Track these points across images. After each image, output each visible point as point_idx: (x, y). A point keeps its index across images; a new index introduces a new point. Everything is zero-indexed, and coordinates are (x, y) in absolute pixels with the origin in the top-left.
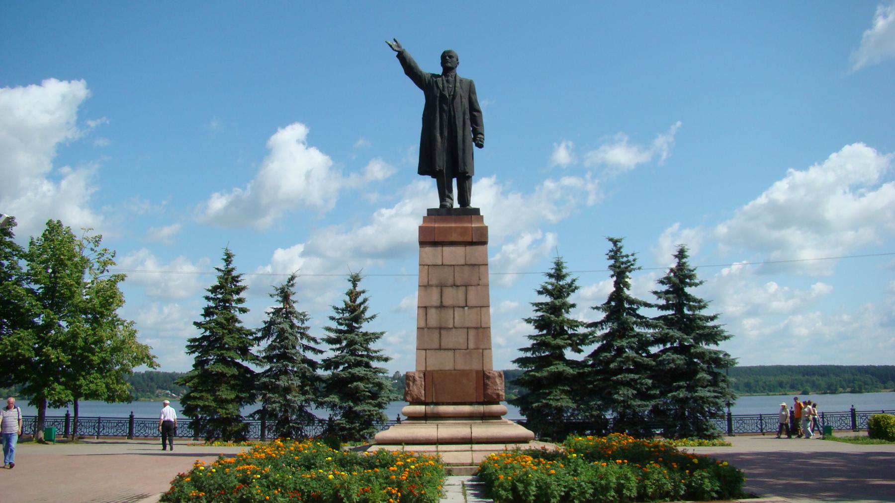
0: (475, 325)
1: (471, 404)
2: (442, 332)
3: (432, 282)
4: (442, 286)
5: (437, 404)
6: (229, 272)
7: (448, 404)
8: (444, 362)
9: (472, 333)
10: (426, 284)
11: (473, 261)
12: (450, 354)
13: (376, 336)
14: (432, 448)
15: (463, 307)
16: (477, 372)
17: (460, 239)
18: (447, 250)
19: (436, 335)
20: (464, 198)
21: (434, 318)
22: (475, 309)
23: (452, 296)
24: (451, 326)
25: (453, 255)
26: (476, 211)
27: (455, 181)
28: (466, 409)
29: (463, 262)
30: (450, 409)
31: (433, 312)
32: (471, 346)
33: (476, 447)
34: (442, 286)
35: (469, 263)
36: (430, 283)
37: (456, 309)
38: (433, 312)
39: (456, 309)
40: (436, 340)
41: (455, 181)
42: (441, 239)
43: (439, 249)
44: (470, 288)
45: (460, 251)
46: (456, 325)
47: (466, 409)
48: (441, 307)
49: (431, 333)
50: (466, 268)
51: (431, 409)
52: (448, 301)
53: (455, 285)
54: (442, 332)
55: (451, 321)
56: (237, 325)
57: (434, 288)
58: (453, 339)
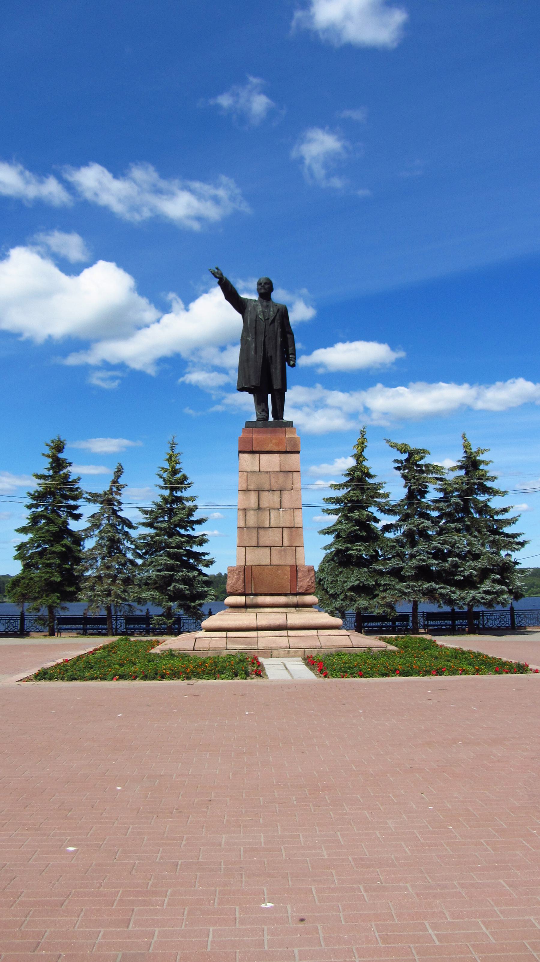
0: (288, 525)
1: (286, 595)
2: (260, 531)
3: (251, 487)
4: (259, 491)
5: (256, 595)
6: (175, 472)
7: (266, 595)
8: (260, 558)
9: (286, 532)
10: (245, 488)
11: (287, 469)
12: (267, 550)
13: (487, 463)
14: (253, 634)
15: (279, 509)
16: (291, 566)
17: (276, 449)
18: (264, 457)
19: (254, 533)
20: (278, 412)
21: (252, 519)
22: (289, 511)
23: (269, 499)
24: (268, 526)
25: (271, 462)
26: (290, 424)
27: (270, 396)
28: (282, 600)
29: (278, 470)
30: (268, 600)
31: (251, 515)
32: (286, 543)
33: (291, 633)
34: (259, 491)
35: (283, 470)
36: (249, 487)
37: (272, 511)
38: (251, 515)
39: (272, 511)
40: (255, 539)
41: (270, 396)
42: (258, 449)
43: (257, 455)
44: (285, 492)
45: (276, 457)
46: (272, 524)
47: (282, 600)
48: (259, 508)
49: (252, 534)
50: (281, 475)
51: (293, 599)
52: (265, 504)
53: (271, 490)
54: (260, 531)
55: (268, 523)
56: (370, 481)
57: (253, 492)
58: (271, 537)
